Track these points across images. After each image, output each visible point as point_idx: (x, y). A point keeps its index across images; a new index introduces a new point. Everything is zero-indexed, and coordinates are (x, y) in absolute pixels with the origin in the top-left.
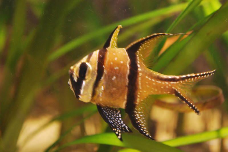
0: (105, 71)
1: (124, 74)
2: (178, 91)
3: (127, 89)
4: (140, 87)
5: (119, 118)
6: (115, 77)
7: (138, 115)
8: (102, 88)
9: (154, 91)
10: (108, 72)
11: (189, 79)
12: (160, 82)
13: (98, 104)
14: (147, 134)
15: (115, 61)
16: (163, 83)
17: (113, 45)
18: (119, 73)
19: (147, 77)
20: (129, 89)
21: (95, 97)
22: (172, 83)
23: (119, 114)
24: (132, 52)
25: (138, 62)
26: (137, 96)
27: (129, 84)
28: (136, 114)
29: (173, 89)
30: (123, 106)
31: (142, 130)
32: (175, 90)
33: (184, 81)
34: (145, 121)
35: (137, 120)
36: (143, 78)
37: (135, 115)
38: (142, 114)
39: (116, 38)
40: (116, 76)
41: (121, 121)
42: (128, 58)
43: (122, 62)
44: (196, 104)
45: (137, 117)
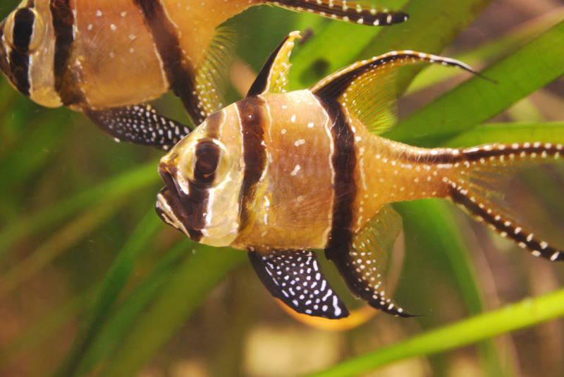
0: (269, 157)
1: (322, 155)
2: (459, 188)
3: (333, 192)
4: (365, 186)
5: (313, 274)
6: (298, 168)
7: (359, 261)
8: (267, 203)
9: (398, 192)
10: (277, 159)
11: (492, 158)
12: (409, 166)
13: (252, 249)
14: (391, 307)
15: (292, 124)
16: (418, 168)
17: (275, 86)
18: (307, 156)
19: (378, 157)
20: (337, 193)
21: (249, 230)
22: (440, 166)
23: (311, 262)
24: (330, 96)
25: (351, 121)
26: (358, 210)
27: (337, 179)
28: (354, 258)
29: (443, 184)
30: (322, 243)
31: (375, 297)
32: (450, 187)
33: (474, 163)
34: (379, 276)
35: (360, 275)
36: (368, 162)
37: (354, 263)
38: (367, 257)
39: (287, 66)
40: (300, 164)
41: (320, 283)
42: (324, 112)
43: (311, 125)
44: (494, 203)
45: (358, 266)
